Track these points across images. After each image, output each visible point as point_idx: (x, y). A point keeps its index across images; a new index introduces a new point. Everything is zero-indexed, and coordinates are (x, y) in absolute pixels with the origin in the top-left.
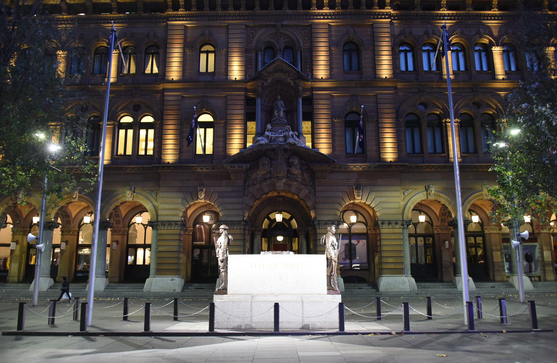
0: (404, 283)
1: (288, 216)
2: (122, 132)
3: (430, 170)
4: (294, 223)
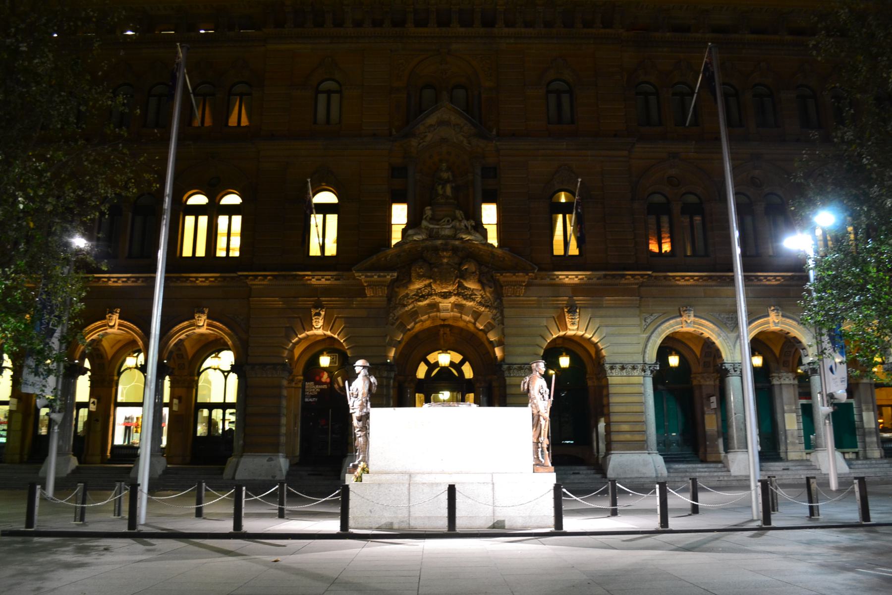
0: (646, 464)
1: (457, 358)
2: (190, 220)
3: (687, 283)
4: (468, 372)
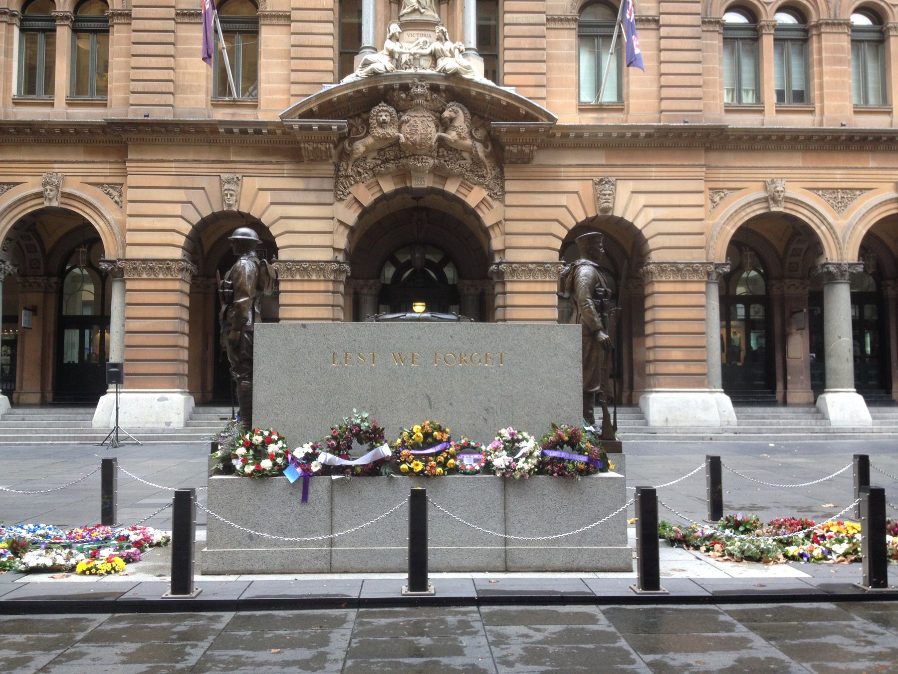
0: (706, 408)
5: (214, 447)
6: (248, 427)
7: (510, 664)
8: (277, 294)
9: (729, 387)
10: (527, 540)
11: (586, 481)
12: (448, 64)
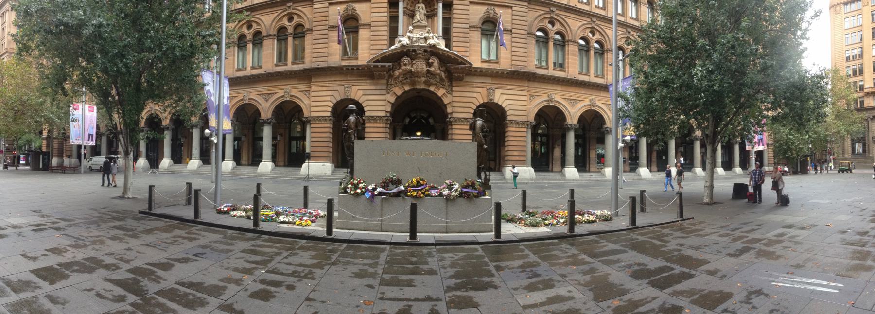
5: (341, 184)
6: (352, 178)
7: (445, 268)
8: (364, 128)
9: (533, 166)
10: (454, 222)
11: (478, 199)
12: (431, 42)
